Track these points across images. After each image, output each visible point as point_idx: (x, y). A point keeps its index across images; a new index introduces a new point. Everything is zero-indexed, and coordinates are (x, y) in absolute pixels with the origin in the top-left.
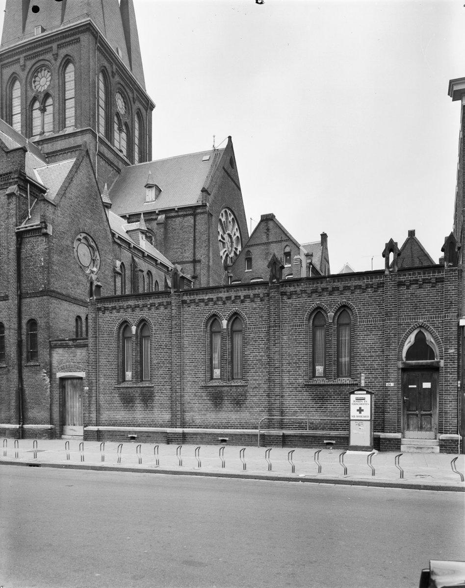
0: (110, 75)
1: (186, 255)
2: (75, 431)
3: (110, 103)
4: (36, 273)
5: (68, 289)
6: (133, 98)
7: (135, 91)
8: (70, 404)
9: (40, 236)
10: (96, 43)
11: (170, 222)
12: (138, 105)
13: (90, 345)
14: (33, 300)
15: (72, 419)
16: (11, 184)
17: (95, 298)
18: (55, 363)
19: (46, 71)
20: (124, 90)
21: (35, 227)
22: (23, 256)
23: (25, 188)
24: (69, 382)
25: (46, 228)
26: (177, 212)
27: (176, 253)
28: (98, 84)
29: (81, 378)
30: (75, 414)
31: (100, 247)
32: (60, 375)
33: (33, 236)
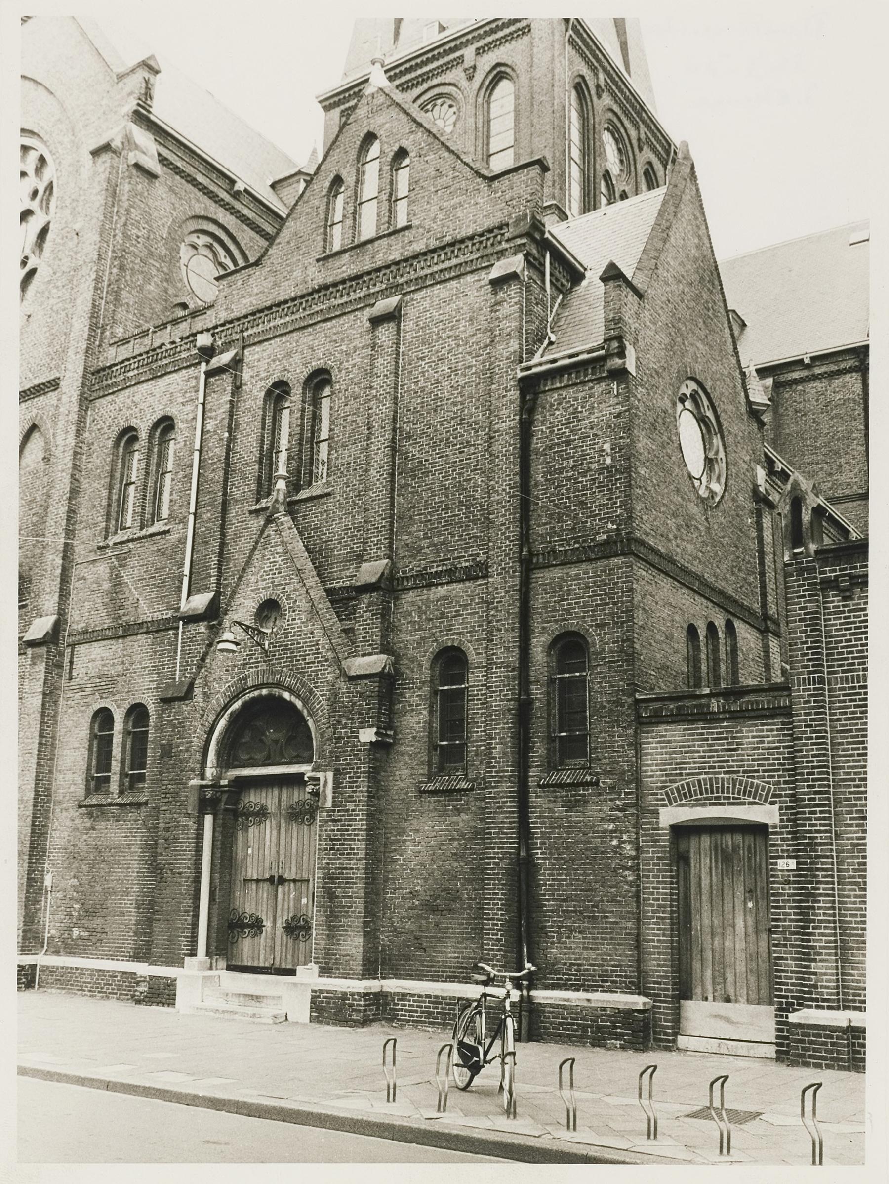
0: (593, 92)
1: (843, 478)
2: (728, 1020)
3: (590, 150)
4: (584, 488)
5: (670, 540)
6: (639, 140)
7: (642, 126)
8: (706, 922)
9: (600, 380)
10: (567, 30)
11: (787, 396)
12: (647, 154)
13: (799, 708)
14: (573, 572)
15: (720, 978)
16: (501, 254)
17: (813, 547)
18: (653, 770)
19: (446, 106)
20: (619, 125)
21: (585, 356)
22: (537, 443)
23: (540, 264)
24: (706, 841)
25: (621, 354)
26: (808, 367)
28: (570, 111)
29: (760, 830)
30: (728, 959)
31: (725, 424)
32: (671, 815)
33: (576, 384)
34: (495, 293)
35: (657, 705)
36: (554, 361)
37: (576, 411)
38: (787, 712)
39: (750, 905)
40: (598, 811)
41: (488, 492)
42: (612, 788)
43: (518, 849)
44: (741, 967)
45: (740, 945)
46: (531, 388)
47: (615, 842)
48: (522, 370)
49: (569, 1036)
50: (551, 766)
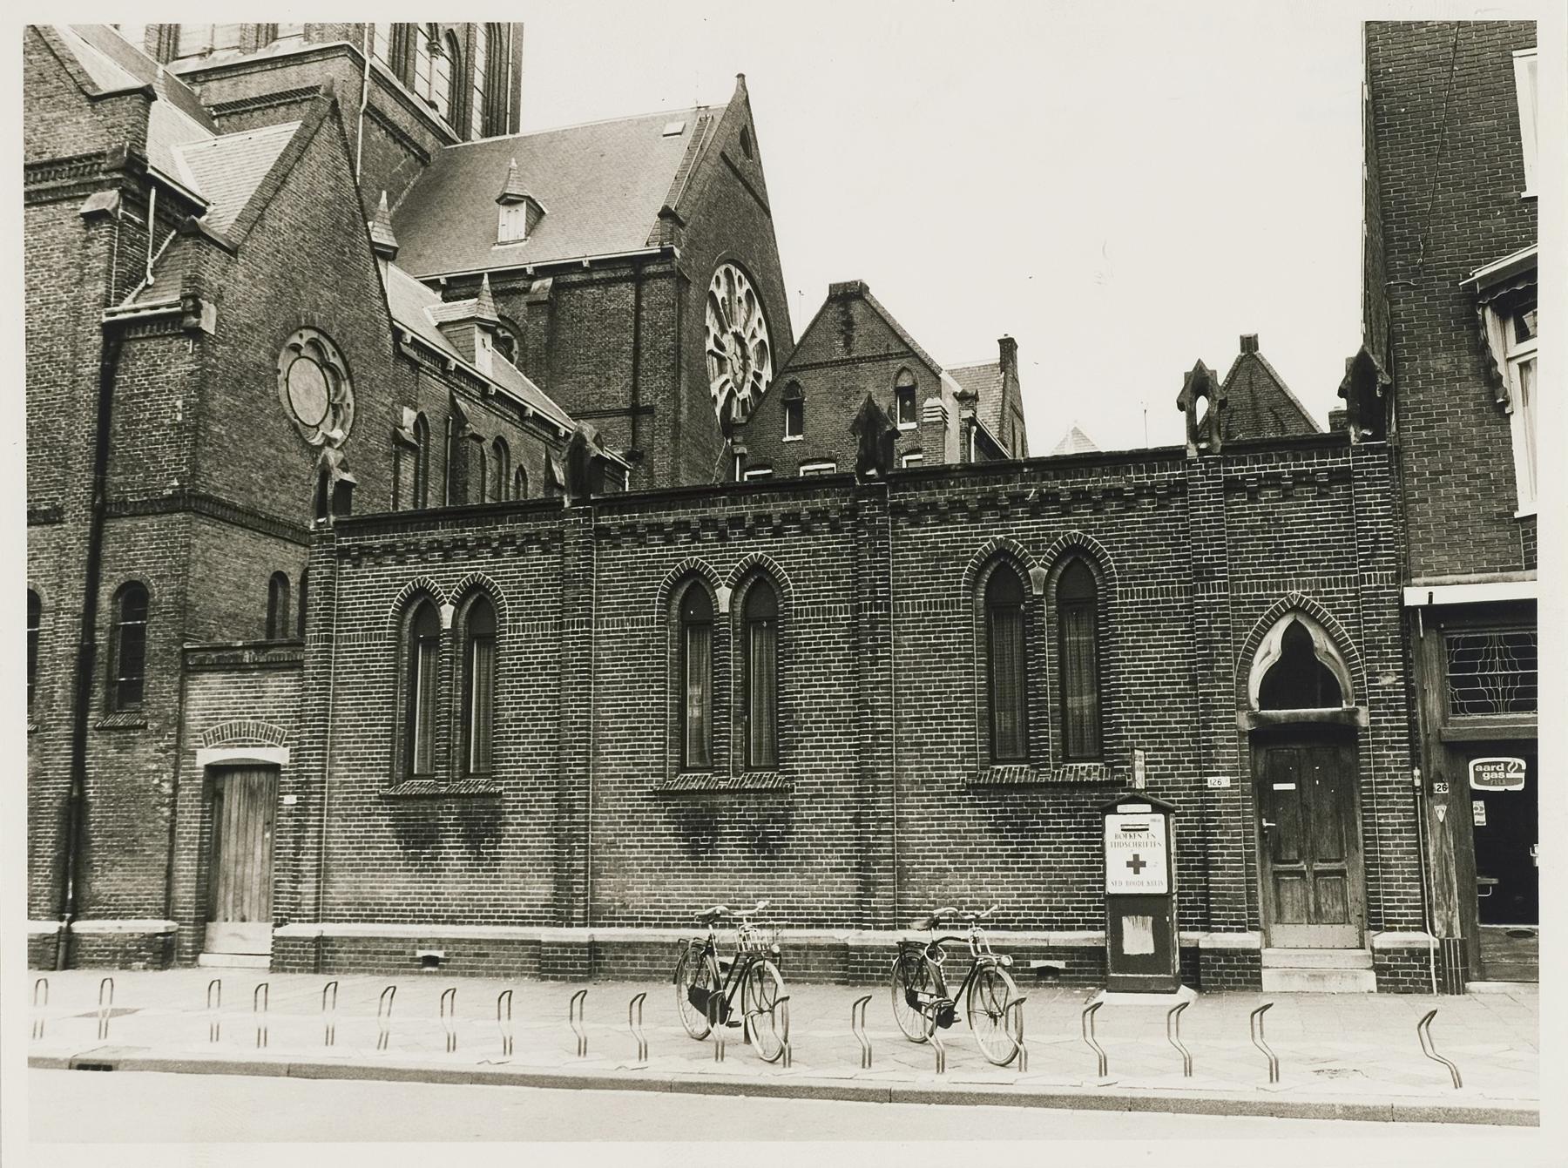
1: (611, 392)
2: (242, 938)
8: (233, 852)
9: (177, 336)
16: (99, 186)
22: (118, 393)
24: (238, 778)
25: (197, 314)
27: (583, 385)
29: (274, 769)
30: (247, 883)
32: (208, 756)
33: (156, 337)
34: (87, 229)
35: (201, 655)
36: (137, 310)
37: (155, 364)
38: (297, 665)
39: (268, 835)
40: (146, 753)
41: (70, 435)
42: (158, 731)
43: (70, 789)
44: (256, 892)
45: (257, 870)
46: (116, 336)
47: (156, 781)
48: (108, 315)
49: (101, 962)
50: (108, 710)
